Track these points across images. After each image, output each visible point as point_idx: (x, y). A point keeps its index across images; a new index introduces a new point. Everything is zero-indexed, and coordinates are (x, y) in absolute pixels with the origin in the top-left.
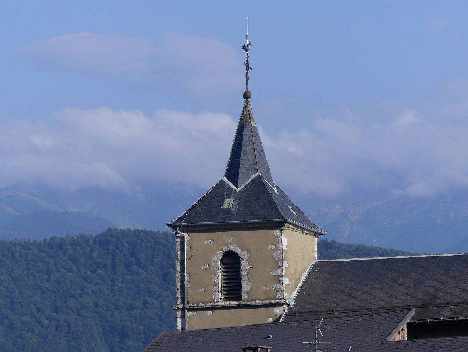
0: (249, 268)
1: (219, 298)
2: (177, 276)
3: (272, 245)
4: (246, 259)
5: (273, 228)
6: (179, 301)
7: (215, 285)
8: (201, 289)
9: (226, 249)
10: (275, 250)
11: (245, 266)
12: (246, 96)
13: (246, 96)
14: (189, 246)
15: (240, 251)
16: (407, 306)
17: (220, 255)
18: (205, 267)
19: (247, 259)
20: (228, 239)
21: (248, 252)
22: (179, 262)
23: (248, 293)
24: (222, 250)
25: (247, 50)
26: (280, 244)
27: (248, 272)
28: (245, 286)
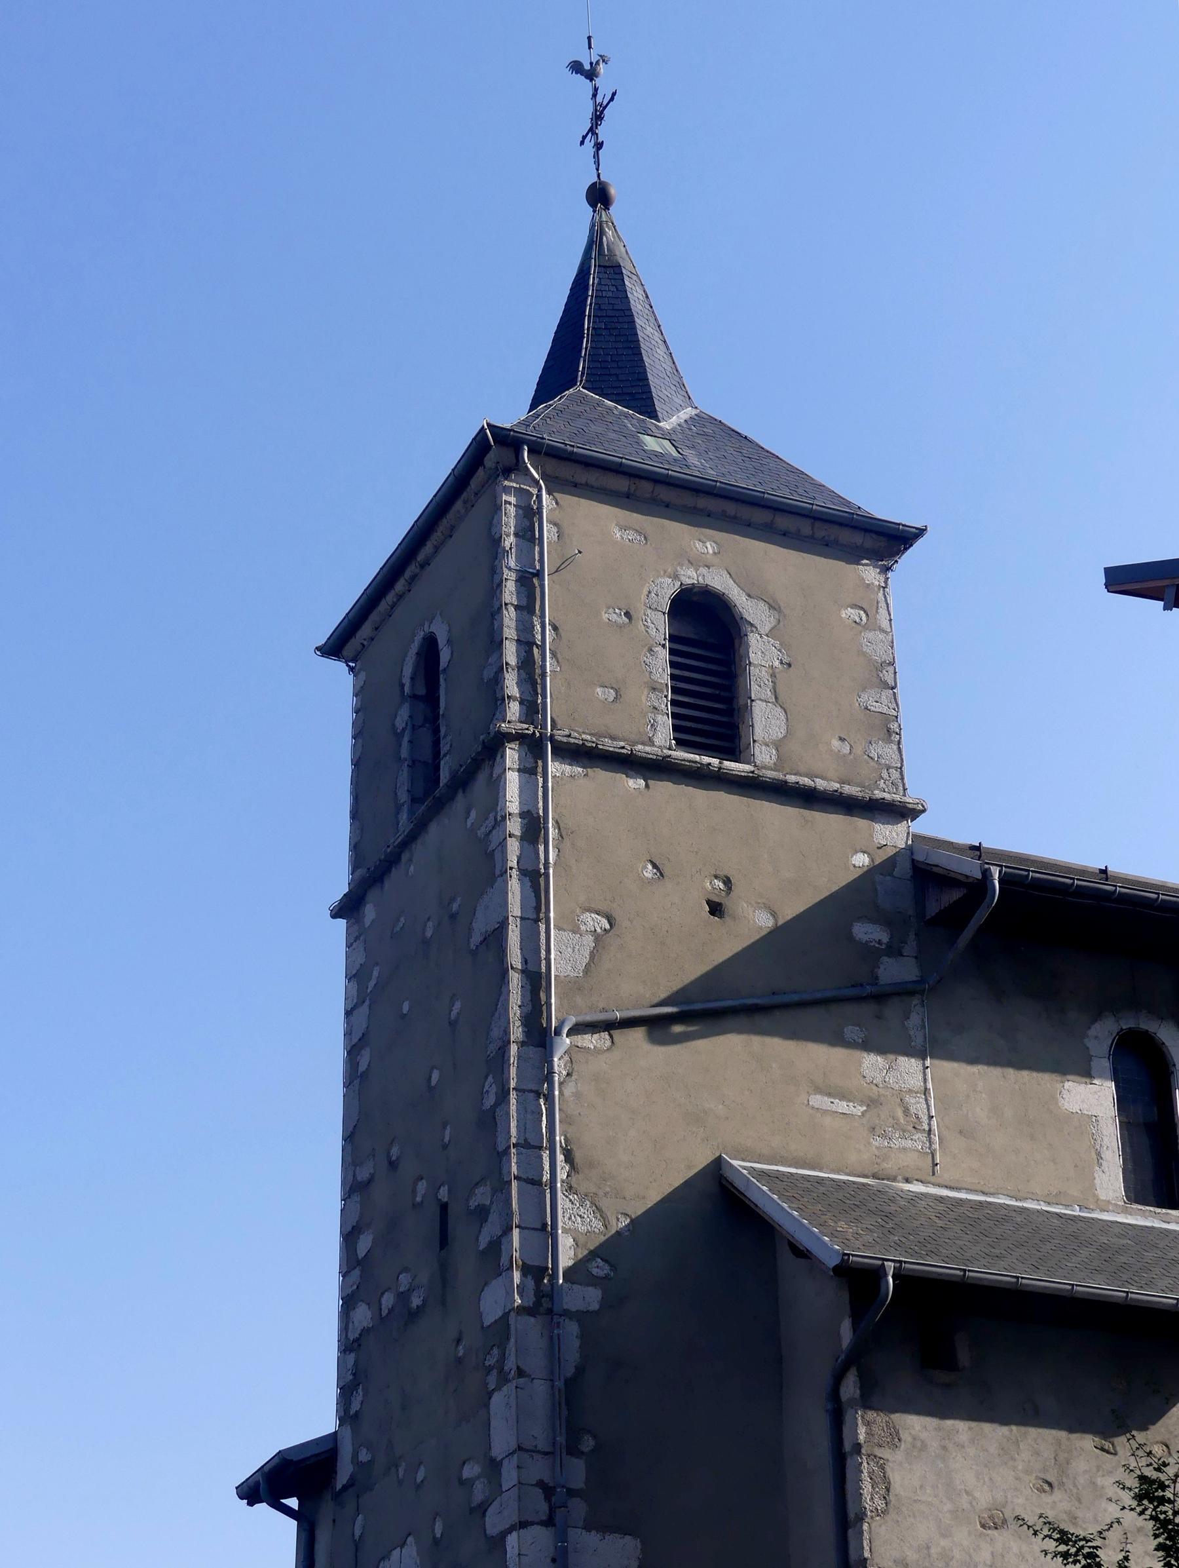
0: (777, 663)
1: (661, 738)
2: (506, 621)
3: (855, 606)
4: (765, 629)
5: (854, 555)
6: (514, 710)
7: (654, 689)
8: (599, 690)
9: (690, 576)
10: (866, 627)
11: (761, 653)
12: (599, 196)
13: (599, 196)
14: (555, 530)
15: (744, 598)
16: (925, 1074)
17: (668, 590)
18: (614, 617)
19: (767, 629)
20: (699, 545)
21: (771, 607)
22: (512, 576)
23: (778, 745)
24: (676, 577)
25: (591, 75)
26: (883, 611)
27: (773, 675)
28: (765, 723)
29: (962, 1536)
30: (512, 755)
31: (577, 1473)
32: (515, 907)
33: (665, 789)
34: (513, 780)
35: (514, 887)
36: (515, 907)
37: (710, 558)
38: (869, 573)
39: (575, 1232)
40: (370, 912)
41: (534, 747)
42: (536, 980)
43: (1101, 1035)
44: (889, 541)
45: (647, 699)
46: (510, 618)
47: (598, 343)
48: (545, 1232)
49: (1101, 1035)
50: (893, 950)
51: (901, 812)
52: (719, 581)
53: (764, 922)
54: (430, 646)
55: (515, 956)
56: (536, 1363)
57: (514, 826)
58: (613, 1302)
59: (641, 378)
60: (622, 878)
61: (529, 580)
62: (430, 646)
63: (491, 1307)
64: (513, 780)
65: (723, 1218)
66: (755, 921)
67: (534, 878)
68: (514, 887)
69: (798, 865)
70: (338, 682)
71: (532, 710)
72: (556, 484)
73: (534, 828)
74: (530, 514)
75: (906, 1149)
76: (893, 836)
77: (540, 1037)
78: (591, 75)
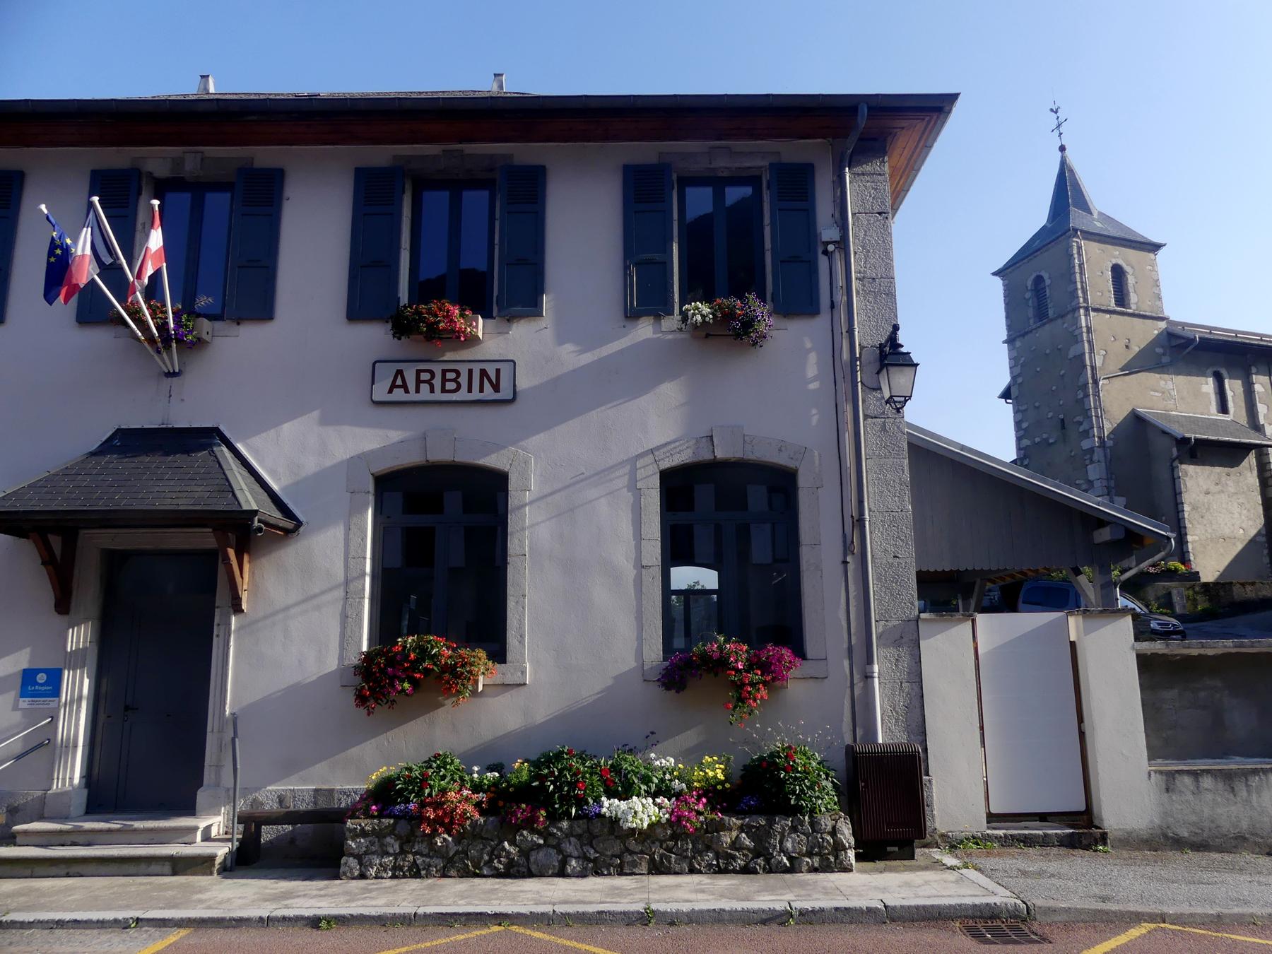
5: (1149, 251)
9: (1114, 261)
11: (1131, 280)
12: (1062, 149)
13: (1062, 149)
25: (1056, 112)
28: (1133, 298)
29: (1202, 496)
30: (1082, 311)
31: (1112, 483)
32: (1087, 350)
33: (1114, 316)
34: (1083, 318)
35: (1086, 345)
36: (1087, 350)
37: (1119, 255)
38: (1152, 255)
39: (1108, 427)
40: (1018, 344)
41: (1087, 309)
42: (1093, 368)
43: (1210, 371)
44: (1155, 247)
45: (1107, 294)
46: (1078, 276)
47: (1067, 192)
48: (1101, 428)
49: (1210, 371)
50: (1164, 354)
51: (1162, 319)
52: (1120, 262)
53: (1137, 349)
54: (1039, 279)
55: (1088, 362)
56: (1102, 459)
57: (1084, 330)
58: (1115, 444)
59: (1087, 204)
60: (1109, 340)
61: (1081, 265)
62: (1039, 279)
63: (1086, 444)
64: (1083, 318)
65: (1137, 422)
66: (1136, 349)
67: (1090, 342)
68: (1086, 345)
69: (1145, 334)
70: (998, 283)
71: (1086, 300)
72: (1084, 239)
73: (1089, 330)
74: (1079, 248)
75: (1170, 404)
76: (1163, 325)
77: (1096, 382)
78: (1056, 112)
